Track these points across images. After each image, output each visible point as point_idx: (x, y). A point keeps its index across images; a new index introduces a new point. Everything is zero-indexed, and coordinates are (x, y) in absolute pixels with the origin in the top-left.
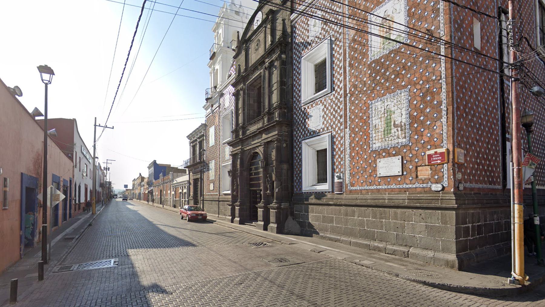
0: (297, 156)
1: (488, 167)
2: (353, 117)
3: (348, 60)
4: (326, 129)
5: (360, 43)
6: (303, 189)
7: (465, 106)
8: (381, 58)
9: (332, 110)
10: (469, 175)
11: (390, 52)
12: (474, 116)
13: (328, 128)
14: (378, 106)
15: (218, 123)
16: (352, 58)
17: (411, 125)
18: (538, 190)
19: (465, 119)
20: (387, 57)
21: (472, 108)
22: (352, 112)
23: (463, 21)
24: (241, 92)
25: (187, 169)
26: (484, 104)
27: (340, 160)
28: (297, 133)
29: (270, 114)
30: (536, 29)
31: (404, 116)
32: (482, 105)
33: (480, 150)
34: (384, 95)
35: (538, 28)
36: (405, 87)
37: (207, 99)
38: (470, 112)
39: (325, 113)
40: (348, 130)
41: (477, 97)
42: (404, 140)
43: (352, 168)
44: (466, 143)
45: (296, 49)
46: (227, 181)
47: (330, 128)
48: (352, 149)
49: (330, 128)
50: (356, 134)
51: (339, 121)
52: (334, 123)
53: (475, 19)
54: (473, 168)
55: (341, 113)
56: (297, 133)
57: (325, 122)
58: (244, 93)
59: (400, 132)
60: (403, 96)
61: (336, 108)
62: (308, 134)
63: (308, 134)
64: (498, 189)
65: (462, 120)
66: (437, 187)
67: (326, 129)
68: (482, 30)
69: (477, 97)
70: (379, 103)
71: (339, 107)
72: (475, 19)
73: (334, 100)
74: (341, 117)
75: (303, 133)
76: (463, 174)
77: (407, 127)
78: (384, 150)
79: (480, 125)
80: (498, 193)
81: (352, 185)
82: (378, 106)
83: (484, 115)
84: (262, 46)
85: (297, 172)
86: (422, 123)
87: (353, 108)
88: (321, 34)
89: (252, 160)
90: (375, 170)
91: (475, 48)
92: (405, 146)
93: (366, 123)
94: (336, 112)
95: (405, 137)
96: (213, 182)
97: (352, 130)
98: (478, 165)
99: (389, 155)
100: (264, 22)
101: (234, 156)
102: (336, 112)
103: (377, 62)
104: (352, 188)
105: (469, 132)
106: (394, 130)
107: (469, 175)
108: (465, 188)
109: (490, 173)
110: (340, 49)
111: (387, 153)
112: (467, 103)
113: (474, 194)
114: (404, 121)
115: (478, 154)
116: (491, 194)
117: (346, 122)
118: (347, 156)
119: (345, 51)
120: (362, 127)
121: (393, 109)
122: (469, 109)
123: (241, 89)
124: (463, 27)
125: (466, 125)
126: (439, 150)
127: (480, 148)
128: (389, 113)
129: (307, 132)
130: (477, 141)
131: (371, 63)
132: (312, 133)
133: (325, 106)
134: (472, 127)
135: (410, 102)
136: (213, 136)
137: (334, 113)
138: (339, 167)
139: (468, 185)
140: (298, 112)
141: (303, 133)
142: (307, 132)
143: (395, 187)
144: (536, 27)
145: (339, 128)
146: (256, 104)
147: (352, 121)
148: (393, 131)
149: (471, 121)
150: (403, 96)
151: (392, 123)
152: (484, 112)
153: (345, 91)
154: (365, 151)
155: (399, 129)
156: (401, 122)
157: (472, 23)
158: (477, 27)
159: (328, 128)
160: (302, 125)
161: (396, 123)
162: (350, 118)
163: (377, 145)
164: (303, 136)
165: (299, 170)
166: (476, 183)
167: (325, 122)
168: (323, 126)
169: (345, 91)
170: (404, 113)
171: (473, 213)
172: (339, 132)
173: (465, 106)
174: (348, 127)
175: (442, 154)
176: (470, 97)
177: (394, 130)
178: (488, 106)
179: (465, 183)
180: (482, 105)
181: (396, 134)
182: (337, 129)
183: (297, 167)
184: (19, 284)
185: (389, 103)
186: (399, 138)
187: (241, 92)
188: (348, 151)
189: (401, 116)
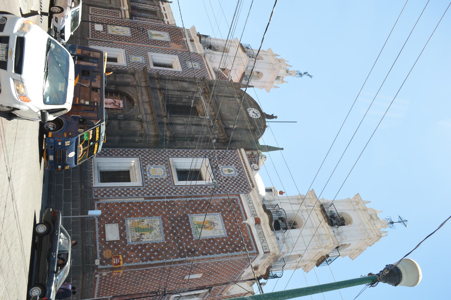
0: (127, 152)
1: (109, 291)
2: (152, 204)
3: (195, 199)
7: (149, 274)
8: (189, 223)
10: (105, 280)
12: (143, 279)
16: (195, 202)
19: (141, 274)
21: (148, 277)
22: (156, 204)
23: (199, 268)
26: (151, 284)
27: (120, 194)
28: (147, 152)
31: (147, 240)
32: (150, 283)
33: (121, 285)
36: (166, 239)
38: (145, 276)
39: (160, 181)
40: (143, 199)
41: (155, 280)
42: (130, 241)
43: (112, 205)
44: (125, 276)
48: (127, 204)
50: (139, 206)
51: (151, 193)
52: (150, 189)
53: (202, 274)
54: (109, 282)
55: (156, 194)
56: (147, 152)
57: (152, 181)
59: (136, 238)
60: (160, 239)
61: (161, 190)
62: (144, 164)
63: (144, 164)
66: (97, 262)
68: (196, 279)
69: (155, 280)
70: (159, 224)
71: (161, 192)
72: (202, 274)
74: (154, 194)
75: (146, 159)
76: (105, 276)
77: (139, 243)
79: (138, 283)
83: (144, 285)
85: (111, 152)
86: (140, 251)
87: (159, 204)
89: (127, 97)
90: (110, 222)
91: (185, 276)
92: (126, 241)
95: (132, 241)
98: (111, 285)
104: (96, 204)
105: (133, 277)
106: (138, 234)
107: (105, 280)
108: (96, 278)
109: (105, 293)
111: (122, 231)
112: (151, 275)
113: (92, 284)
114: (144, 240)
115: (119, 284)
117: (149, 198)
120: (144, 212)
121: (153, 233)
122: (147, 276)
124: (196, 268)
125: (137, 275)
126: (121, 262)
127: (122, 285)
128: (150, 229)
129: (146, 163)
130: (127, 283)
131: (188, 217)
132: (144, 168)
133: (165, 181)
134: (136, 279)
135: (156, 244)
138: (114, 194)
139: (98, 280)
141: (146, 159)
142: (146, 163)
143: (97, 236)
145: (145, 193)
146: (182, 104)
149: (140, 278)
150: (160, 239)
151: (143, 233)
152: (146, 285)
157: (200, 273)
158: (199, 276)
159: (147, 183)
161: (143, 235)
162: (152, 202)
164: (143, 159)
165: (113, 153)
166: (99, 285)
167: (152, 181)
168: (149, 179)
170: (149, 240)
172: (142, 193)
173: (149, 274)
174: (145, 201)
175: (119, 264)
176: (155, 276)
177: (138, 234)
178: (150, 287)
180: (150, 283)
181: (135, 236)
182: (145, 191)
183: (116, 152)
184: (36, 16)
185: (157, 230)
188: (127, 200)
189: (148, 238)
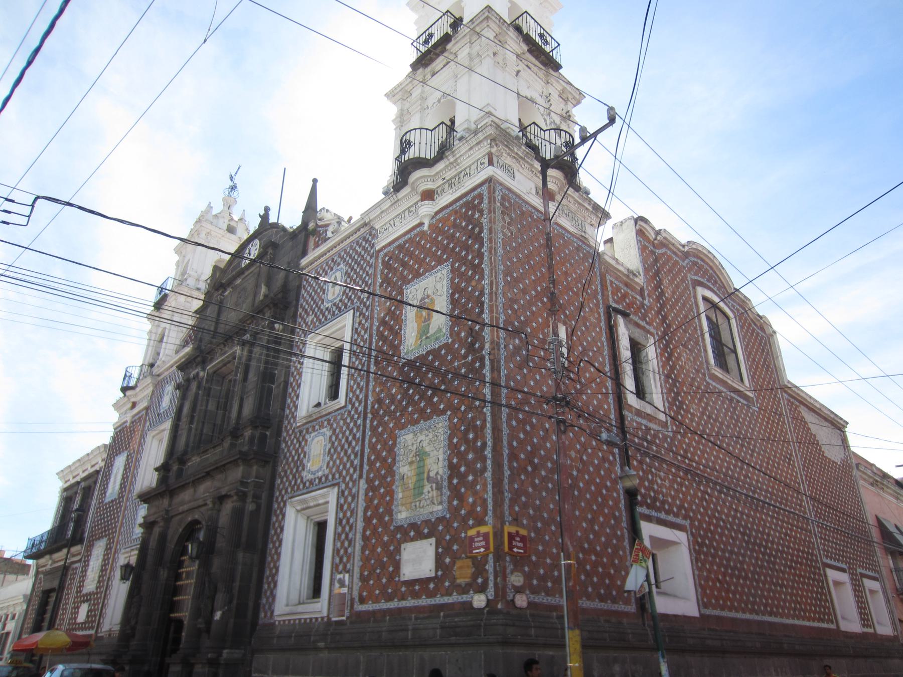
4: (330, 477)
5: (391, 329)
6: (276, 613)
9: (343, 441)
11: (428, 353)
13: (334, 475)
14: (408, 440)
15: (136, 446)
17: (450, 478)
18: (187, 546)
20: (423, 358)
22: (373, 447)
24: (194, 386)
25: (30, 562)
29: (235, 434)
30: (703, 339)
31: (441, 464)
34: (417, 422)
35: (707, 336)
37: (124, 389)
42: (440, 507)
45: (303, 318)
46: (120, 591)
47: (337, 476)
49: (337, 476)
58: (199, 387)
60: (440, 426)
61: (350, 438)
62: (301, 486)
63: (301, 486)
64: (626, 614)
65: (523, 477)
67: (330, 477)
70: (411, 436)
73: (348, 421)
76: (528, 577)
78: (413, 526)
80: (625, 621)
81: (362, 601)
82: (408, 440)
84: (250, 299)
88: (341, 300)
92: (440, 520)
93: (391, 471)
94: (350, 444)
95: (441, 503)
96: (87, 598)
97: (369, 481)
99: (420, 536)
100: (261, 256)
101: (148, 525)
102: (350, 444)
103: (410, 363)
110: (365, 333)
111: (416, 531)
114: (441, 472)
116: (606, 621)
118: (359, 536)
119: (371, 336)
121: (427, 449)
123: (194, 378)
126: (483, 529)
132: (307, 484)
136: (119, 477)
137: (346, 446)
140: (290, 438)
142: (299, 481)
144: (702, 334)
147: (371, 464)
148: (425, 491)
150: (440, 426)
151: (426, 475)
153: (366, 407)
154: (386, 526)
155: (434, 485)
156: (437, 473)
159: (334, 475)
160: (292, 465)
163: (402, 516)
168: (327, 472)
169: (366, 407)
170: (441, 459)
171: (553, 657)
179: (533, 593)
186: (433, 505)
187: (194, 386)
189: (437, 464)
